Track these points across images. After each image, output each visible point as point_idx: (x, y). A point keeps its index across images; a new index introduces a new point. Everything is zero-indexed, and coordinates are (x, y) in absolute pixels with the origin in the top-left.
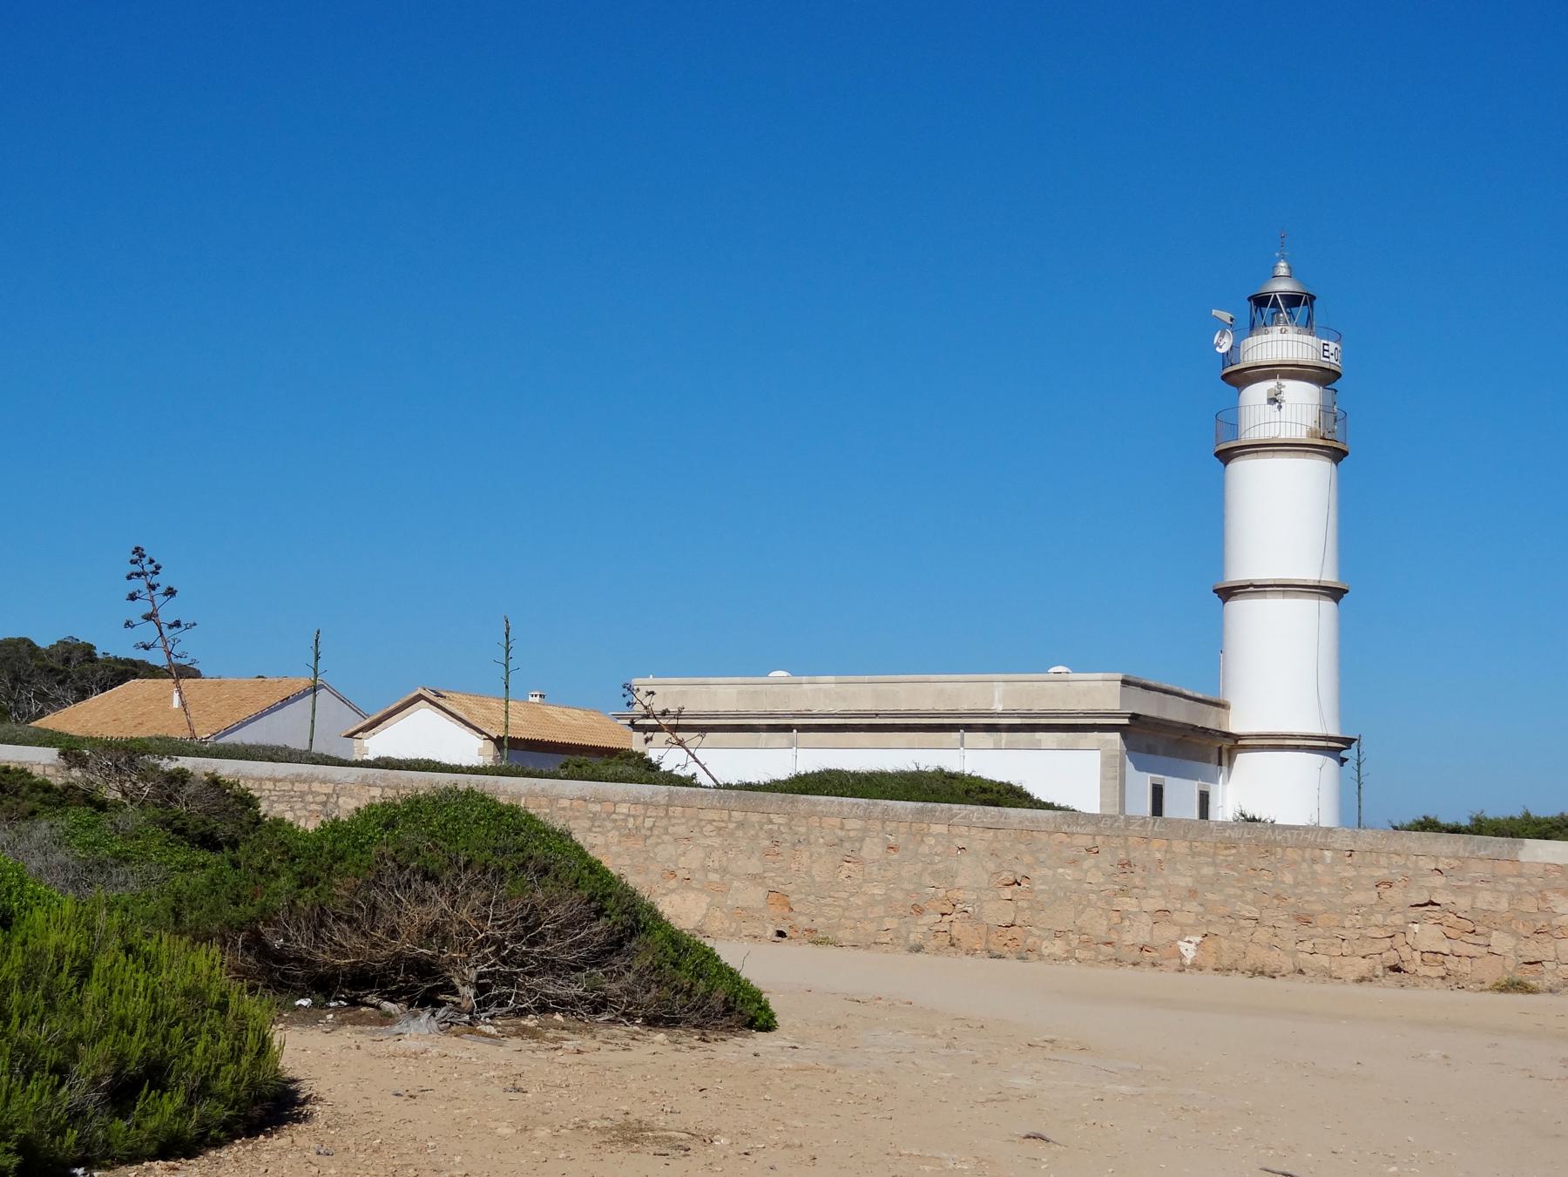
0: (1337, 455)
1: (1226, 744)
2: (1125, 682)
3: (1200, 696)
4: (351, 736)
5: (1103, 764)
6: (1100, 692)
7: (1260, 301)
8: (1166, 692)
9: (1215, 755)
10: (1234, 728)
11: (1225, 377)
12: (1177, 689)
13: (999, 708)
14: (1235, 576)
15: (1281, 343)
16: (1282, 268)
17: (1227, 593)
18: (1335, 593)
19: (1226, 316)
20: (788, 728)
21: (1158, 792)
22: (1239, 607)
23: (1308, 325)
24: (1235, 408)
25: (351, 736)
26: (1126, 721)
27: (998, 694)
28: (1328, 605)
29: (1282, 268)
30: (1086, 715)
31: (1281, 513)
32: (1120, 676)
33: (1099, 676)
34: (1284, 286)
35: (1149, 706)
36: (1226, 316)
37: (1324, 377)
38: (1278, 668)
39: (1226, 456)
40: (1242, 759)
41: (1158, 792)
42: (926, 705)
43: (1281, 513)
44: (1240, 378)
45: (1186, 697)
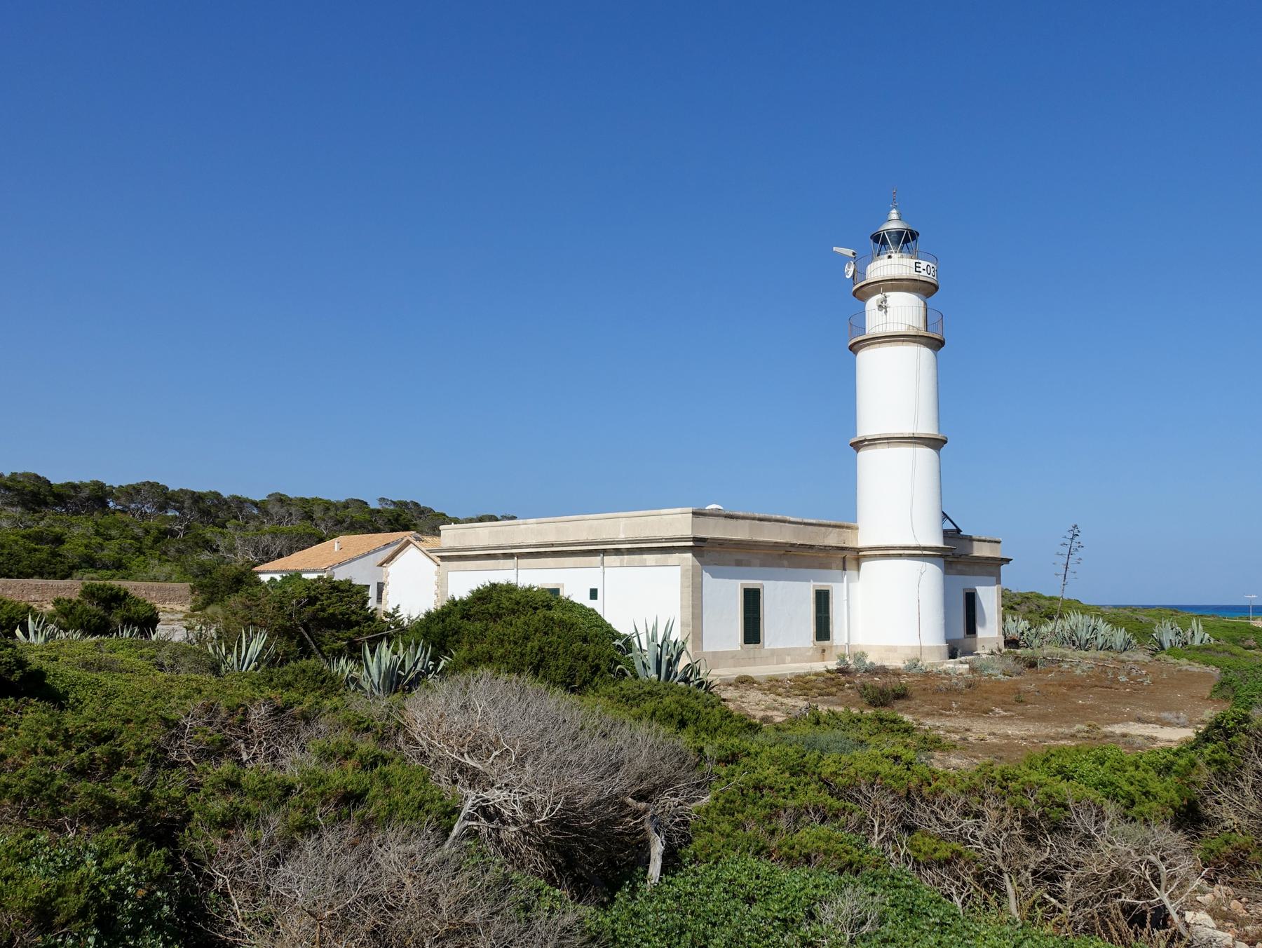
0: (936, 344)
1: (849, 555)
2: (694, 513)
4: (381, 565)
5: (682, 576)
6: (676, 522)
8: (761, 520)
11: (854, 294)
12: (750, 514)
13: (622, 536)
14: (864, 431)
15: (893, 265)
16: (894, 214)
17: (858, 446)
18: (936, 443)
19: (848, 252)
21: (752, 600)
22: (865, 455)
23: (913, 254)
24: (863, 313)
25: (381, 565)
26: (691, 544)
27: (528, 532)
28: (926, 453)
29: (894, 214)
30: (668, 540)
31: (894, 386)
32: (690, 510)
33: (678, 510)
34: (894, 224)
35: (715, 530)
36: (848, 252)
37: (925, 289)
38: (896, 499)
39: (854, 348)
40: (865, 565)
41: (752, 600)
42: (583, 537)
43: (894, 386)
44: (862, 294)
45: (790, 522)
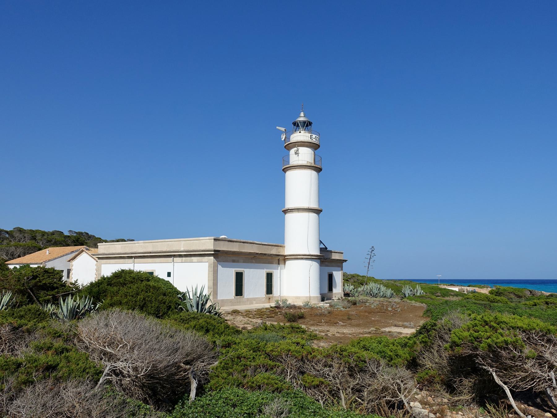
0: (318, 170)
1: (281, 258)
2: (215, 239)
3: (274, 244)
4: (69, 261)
6: (207, 243)
7: (295, 124)
9: (277, 261)
10: (286, 254)
13: (182, 249)
14: (288, 206)
17: (285, 212)
18: (318, 212)
19: (283, 129)
20: (131, 257)
21: (239, 277)
22: (288, 216)
23: (310, 131)
25: (69, 261)
26: (213, 253)
27: (139, 247)
28: (313, 215)
31: (300, 187)
32: (213, 238)
33: (208, 238)
34: (302, 119)
36: (283, 129)
37: (314, 147)
39: (285, 170)
41: (239, 277)
42: (164, 249)
43: (300, 187)
44: (289, 147)
45: (256, 244)
